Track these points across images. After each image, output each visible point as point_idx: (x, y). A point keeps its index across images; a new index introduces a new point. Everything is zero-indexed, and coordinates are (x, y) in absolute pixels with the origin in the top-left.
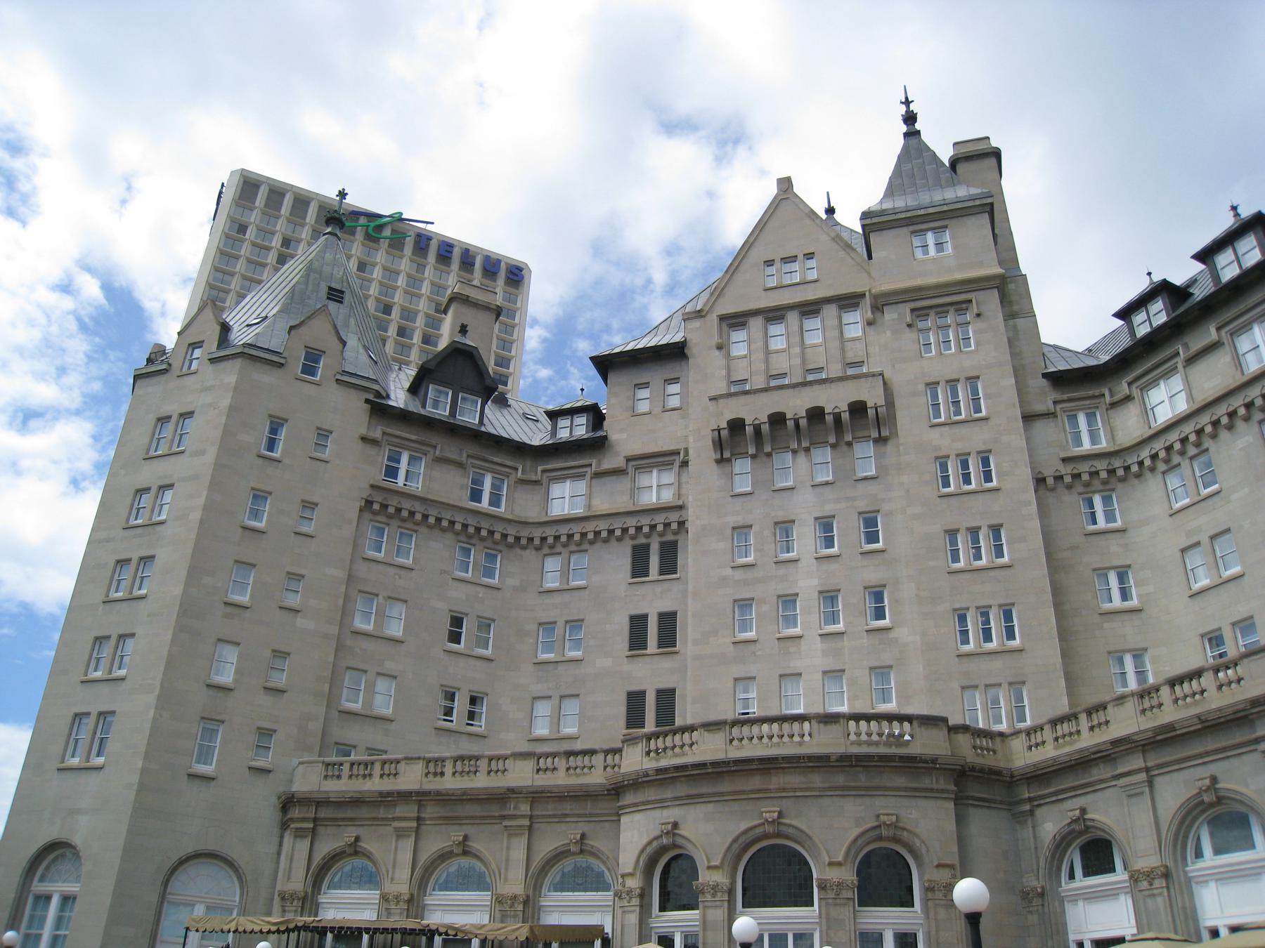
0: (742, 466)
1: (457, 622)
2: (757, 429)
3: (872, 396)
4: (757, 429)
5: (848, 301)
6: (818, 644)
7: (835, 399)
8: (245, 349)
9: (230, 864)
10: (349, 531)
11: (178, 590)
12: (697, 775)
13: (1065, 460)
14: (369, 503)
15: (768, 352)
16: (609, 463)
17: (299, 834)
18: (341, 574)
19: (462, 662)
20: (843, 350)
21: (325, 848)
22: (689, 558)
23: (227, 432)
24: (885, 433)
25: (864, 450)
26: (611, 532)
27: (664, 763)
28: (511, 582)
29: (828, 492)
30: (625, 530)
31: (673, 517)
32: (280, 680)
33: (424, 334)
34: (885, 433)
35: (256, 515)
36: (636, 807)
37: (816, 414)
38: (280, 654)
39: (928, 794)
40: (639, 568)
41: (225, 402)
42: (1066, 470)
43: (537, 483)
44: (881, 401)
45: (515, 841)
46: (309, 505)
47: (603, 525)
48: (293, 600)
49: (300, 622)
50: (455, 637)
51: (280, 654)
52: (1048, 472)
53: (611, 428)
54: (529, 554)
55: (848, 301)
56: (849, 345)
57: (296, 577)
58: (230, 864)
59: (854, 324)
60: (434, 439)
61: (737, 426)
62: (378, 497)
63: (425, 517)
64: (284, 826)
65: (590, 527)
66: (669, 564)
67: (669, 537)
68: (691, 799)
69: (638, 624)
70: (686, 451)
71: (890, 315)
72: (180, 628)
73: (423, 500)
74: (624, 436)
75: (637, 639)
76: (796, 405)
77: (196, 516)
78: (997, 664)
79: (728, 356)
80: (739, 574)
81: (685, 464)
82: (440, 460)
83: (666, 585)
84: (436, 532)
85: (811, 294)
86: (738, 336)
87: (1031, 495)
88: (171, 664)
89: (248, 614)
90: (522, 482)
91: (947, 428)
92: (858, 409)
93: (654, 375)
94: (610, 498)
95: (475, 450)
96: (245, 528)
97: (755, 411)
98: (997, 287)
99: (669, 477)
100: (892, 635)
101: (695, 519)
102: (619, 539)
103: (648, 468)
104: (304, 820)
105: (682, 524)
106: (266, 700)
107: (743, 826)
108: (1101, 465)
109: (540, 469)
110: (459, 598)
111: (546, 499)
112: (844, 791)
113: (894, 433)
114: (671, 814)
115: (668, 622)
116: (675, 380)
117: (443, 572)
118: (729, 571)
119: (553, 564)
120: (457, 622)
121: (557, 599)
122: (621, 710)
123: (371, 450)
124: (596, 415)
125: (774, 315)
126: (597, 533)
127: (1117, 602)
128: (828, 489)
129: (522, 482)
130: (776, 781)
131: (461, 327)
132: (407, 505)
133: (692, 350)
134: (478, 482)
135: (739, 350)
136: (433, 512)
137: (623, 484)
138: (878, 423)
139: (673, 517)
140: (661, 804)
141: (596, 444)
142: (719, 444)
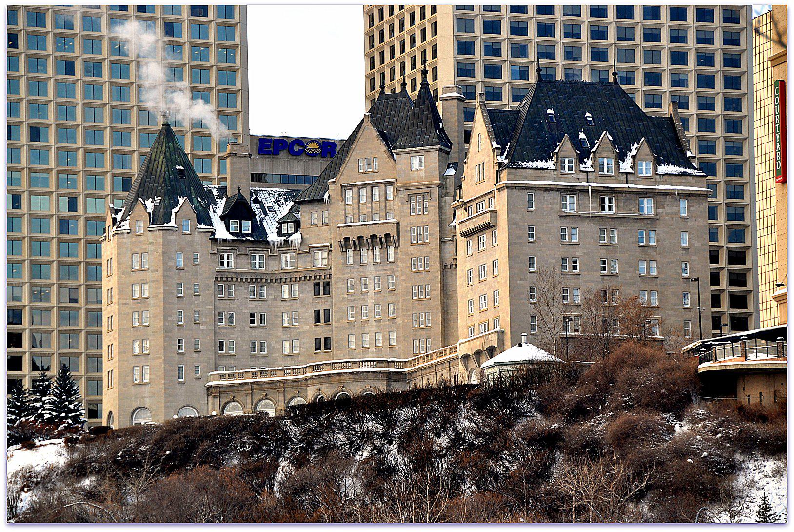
1: (253, 316)
3: (393, 233)
7: (380, 233)
8: (113, 300)
9: (138, 408)
10: (211, 291)
11: (162, 323)
12: (357, 373)
14: (217, 278)
17: (215, 397)
18: (212, 307)
19: (256, 331)
21: (223, 401)
22: (333, 288)
23: (164, 263)
26: (305, 277)
28: (270, 297)
29: (379, 267)
31: (327, 272)
35: (179, 291)
36: (311, 385)
39: (379, 380)
40: (317, 293)
41: (161, 250)
45: (280, 395)
47: (302, 275)
49: (201, 327)
50: (253, 322)
58: (138, 408)
61: (347, 239)
64: (208, 395)
66: (327, 292)
68: (323, 383)
69: (317, 313)
72: (165, 337)
74: (308, 236)
75: (317, 319)
76: (367, 233)
77: (161, 296)
83: (326, 299)
84: (242, 283)
86: (349, 194)
88: (165, 348)
89: (185, 327)
92: (387, 236)
94: (303, 265)
96: (178, 297)
97: (353, 236)
98: (372, 188)
100: (396, 320)
106: (195, 356)
107: (335, 390)
110: (253, 307)
112: (358, 380)
114: (319, 386)
115: (327, 313)
117: (246, 298)
118: (346, 296)
119: (286, 288)
121: (288, 303)
123: (214, 257)
128: (378, 265)
131: (222, 220)
139: (327, 272)
140: (316, 384)
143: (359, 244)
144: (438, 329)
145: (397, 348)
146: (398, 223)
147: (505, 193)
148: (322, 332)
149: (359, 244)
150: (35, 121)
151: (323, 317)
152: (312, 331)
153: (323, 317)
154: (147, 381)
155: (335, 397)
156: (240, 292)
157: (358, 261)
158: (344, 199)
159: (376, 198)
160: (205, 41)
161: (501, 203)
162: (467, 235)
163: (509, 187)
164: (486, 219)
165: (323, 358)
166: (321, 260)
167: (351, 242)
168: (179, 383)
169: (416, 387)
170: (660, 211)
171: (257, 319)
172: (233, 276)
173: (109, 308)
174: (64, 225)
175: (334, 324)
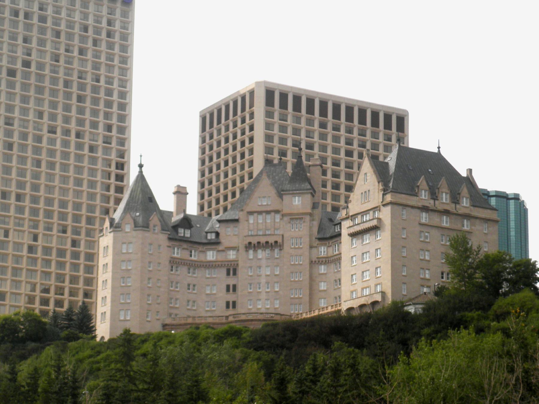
0: (251, 252)
1: (189, 285)
2: (254, 245)
3: (280, 240)
4: (254, 245)
5: (277, 212)
6: (265, 294)
7: (271, 240)
13: (317, 258)
15: (258, 223)
16: (221, 248)
20: (274, 225)
22: (240, 272)
24: (281, 248)
25: (276, 251)
27: (236, 319)
30: (225, 265)
32: (159, 301)
33: (79, 48)
34: (281, 248)
37: (267, 243)
38: (158, 296)
40: (228, 274)
42: (317, 260)
43: (204, 251)
44: (281, 241)
46: (159, 263)
47: (220, 263)
48: (159, 285)
50: (189, 289)
51: (158, 296)
52: (314, 260)
53: (222, 238)
54: (203, 269)
55: (277, 212)
56: (276, 224)
57: (159, 280)
59: (278, 217)
60: (182, 243)
61: (250, 243)
62: (172, 260)
63: (181, 263)
65: (217, 263)
66: (235, 273)
67: (235, 267)
69: (228, 287)
70: (239, 247)
71: (286, 219)
73: (181, 259)
75: (228, 289)
76: (263, 240)
78: (297, 300)
79: (249, 223)
80: (249, 278)
81: (238, 250)
82: (184, 249)
85: (269, 209)
87: (308, 266)
90: (201, 251)
91: (293, 249)
93: (231, 225)
94: (221, 257)
95: (190, 245)
97: (254, 241)
99: (235, 252)
101: (241, 264)
102: (224, 267)
103: (230, 250)
104: (169, 328)
105: (237, 264)
106: (157, 306)
108: (324, 260)
109: (205, 248)
110: (189, 280)
111: (206, 256)
113: (283, 249)
115: (235, 287)
116: (236, 227)
118: (247, 277)
120: (189, 285)
122: (225, 305)
124: (217, 234)
125: (260, 213)
126: (219, 265)
127: (444, 201)
129: (201, 251)
130: (253, 322)
132: (178, 261)
133: (240, 220)
134: (191, 252)
135: (251, 221)
136: (183, 262)
137: (224, 254)
138: (280, 246)
139: (236, 263)
141: (218, 243)
142: (246, 247)
143: (258, 246)
144: (307, 299)
145: (279, 309)
146: (283, 236)
147: (389, 208)
148: (231, 297)
149: (258, 246)
150: (20, 191)
151: (232, 289)
152: (224, 297)
153: (232, 289)
154: (128, 318)
155: (407, 302)
156: (183, 270)
157: (255, 257)
158: (248, 221)
159: (268, 221)
160: (22, 216)
161: (386, 214)
162: (353, 235)
163: (391, 203)
164: (374, 223)
165: (231, 311)
166: (232, 255)
167: (253, 245)
168: (147, 321)
169: (143, 358)
170: (473, 228)
171: (191, 287)
172: (180, 261)
173: (104, 275)
174: (31, 249)
175: (239, 293)
